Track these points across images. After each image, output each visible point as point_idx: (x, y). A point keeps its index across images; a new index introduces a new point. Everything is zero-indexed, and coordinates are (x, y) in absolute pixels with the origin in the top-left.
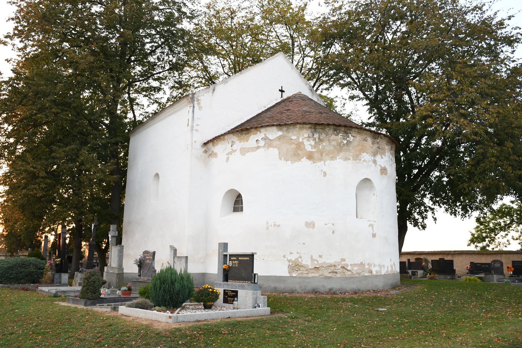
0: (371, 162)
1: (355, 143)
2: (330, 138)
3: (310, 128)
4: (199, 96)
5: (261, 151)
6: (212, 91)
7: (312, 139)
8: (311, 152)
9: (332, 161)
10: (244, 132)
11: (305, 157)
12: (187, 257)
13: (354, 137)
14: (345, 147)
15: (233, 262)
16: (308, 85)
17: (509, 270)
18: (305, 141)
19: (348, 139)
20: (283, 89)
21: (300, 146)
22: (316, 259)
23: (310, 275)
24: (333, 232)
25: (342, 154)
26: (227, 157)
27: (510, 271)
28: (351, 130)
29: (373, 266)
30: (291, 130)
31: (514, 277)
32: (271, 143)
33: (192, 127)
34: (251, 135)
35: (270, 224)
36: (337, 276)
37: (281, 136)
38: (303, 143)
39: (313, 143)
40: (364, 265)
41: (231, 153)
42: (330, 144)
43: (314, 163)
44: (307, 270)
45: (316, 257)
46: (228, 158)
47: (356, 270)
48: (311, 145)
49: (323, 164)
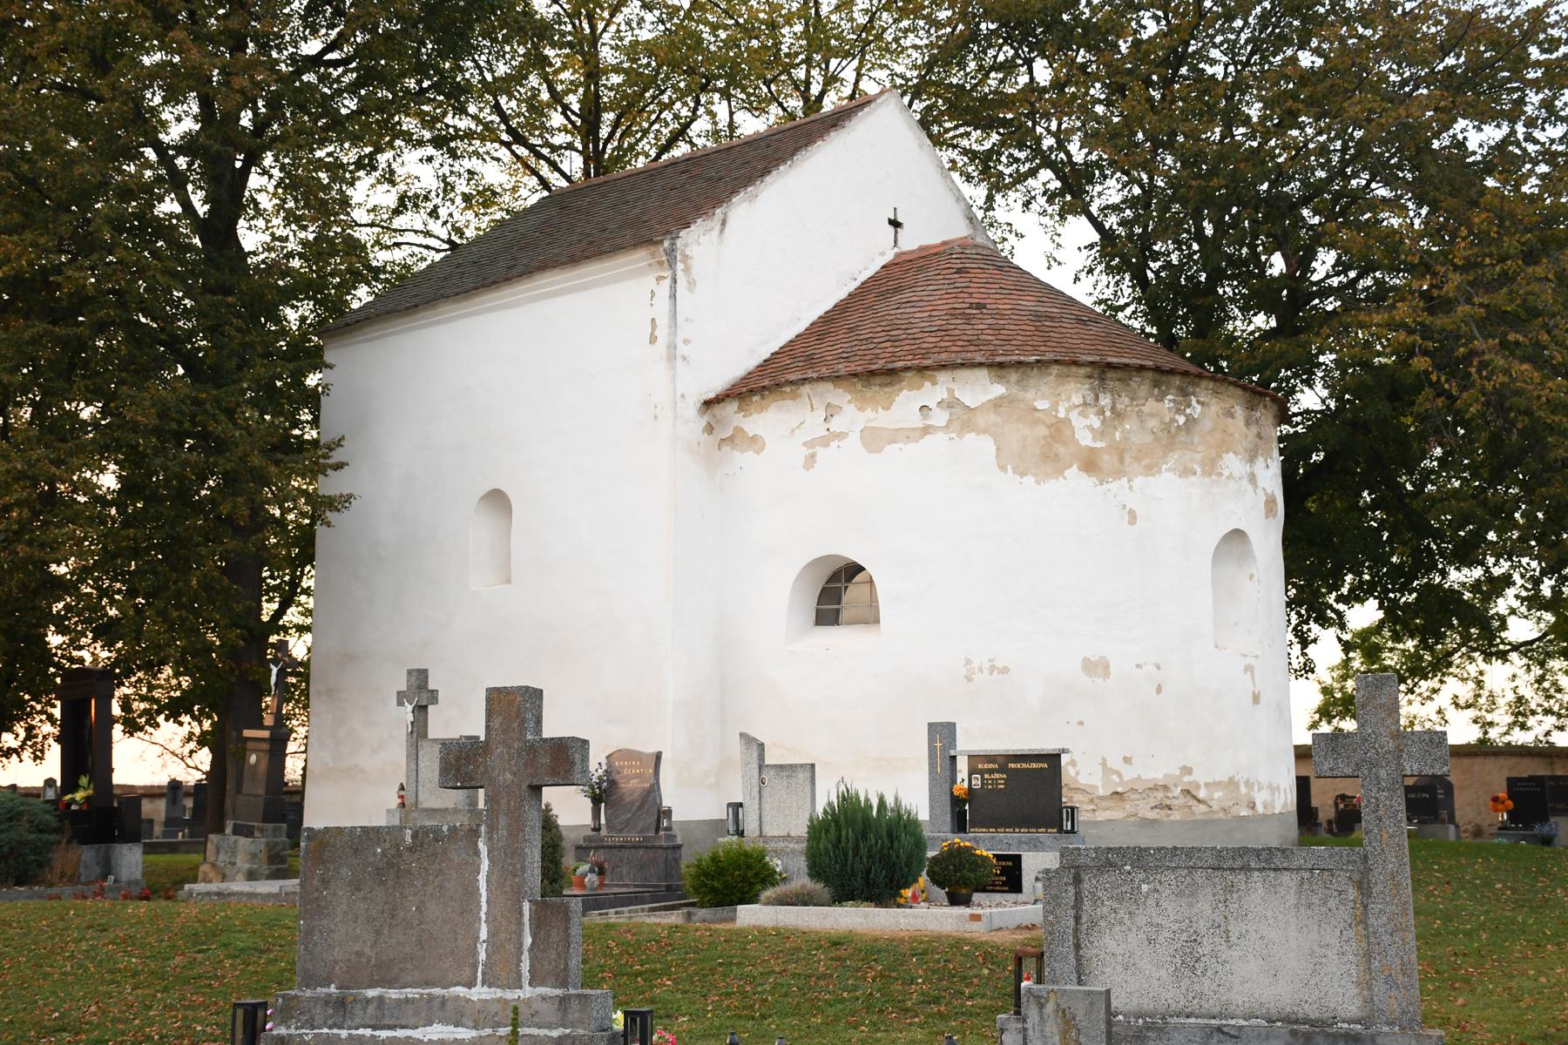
0: (1245, 481)
1: (1207, 424)
2: (1143, 408)
3: (1089, 377)
4: (686, 245)
5: (937, 441)
6: (718, 227)
7: (1095, 410)
8: (1092, 450)
9: (1150, 478)
10: (878, 380)
11: (1075, 466)
12: (813, 766)
13: (1202, 404)
14: (1182, 437)
15: (986, 776)
16: (962, 204)
17: (1500, 806)
18: (1074, 415)
19: (1188, 411)
20: (899, 220)
21: (1059, 430)
22: (1115, 768)
23: (1101, 816)
24: (1159, 690)
25: (1174, 458)
26: (807, 452)
27: (1502, 811)
28: (1198, 386)
29: (1256, 787)
30: (1032, 382)
31: (1512, 829)
32: (969, 420)
33: (672, 347)
34: (901, 390)
35: (976, 665)
36: (1172, 818)
37: (1002, 397)
38: (1067, 421)
39: (1096, 422)
40: (1237, 785)
41: (824, 442)
42: (1142, 427)
43: (1101, 484)
44: (1092, 801)
45: (1115, 762)
46: (813, 456)
47: (1218, 800)
48: (1091, 428)
49: (1127, 486)
